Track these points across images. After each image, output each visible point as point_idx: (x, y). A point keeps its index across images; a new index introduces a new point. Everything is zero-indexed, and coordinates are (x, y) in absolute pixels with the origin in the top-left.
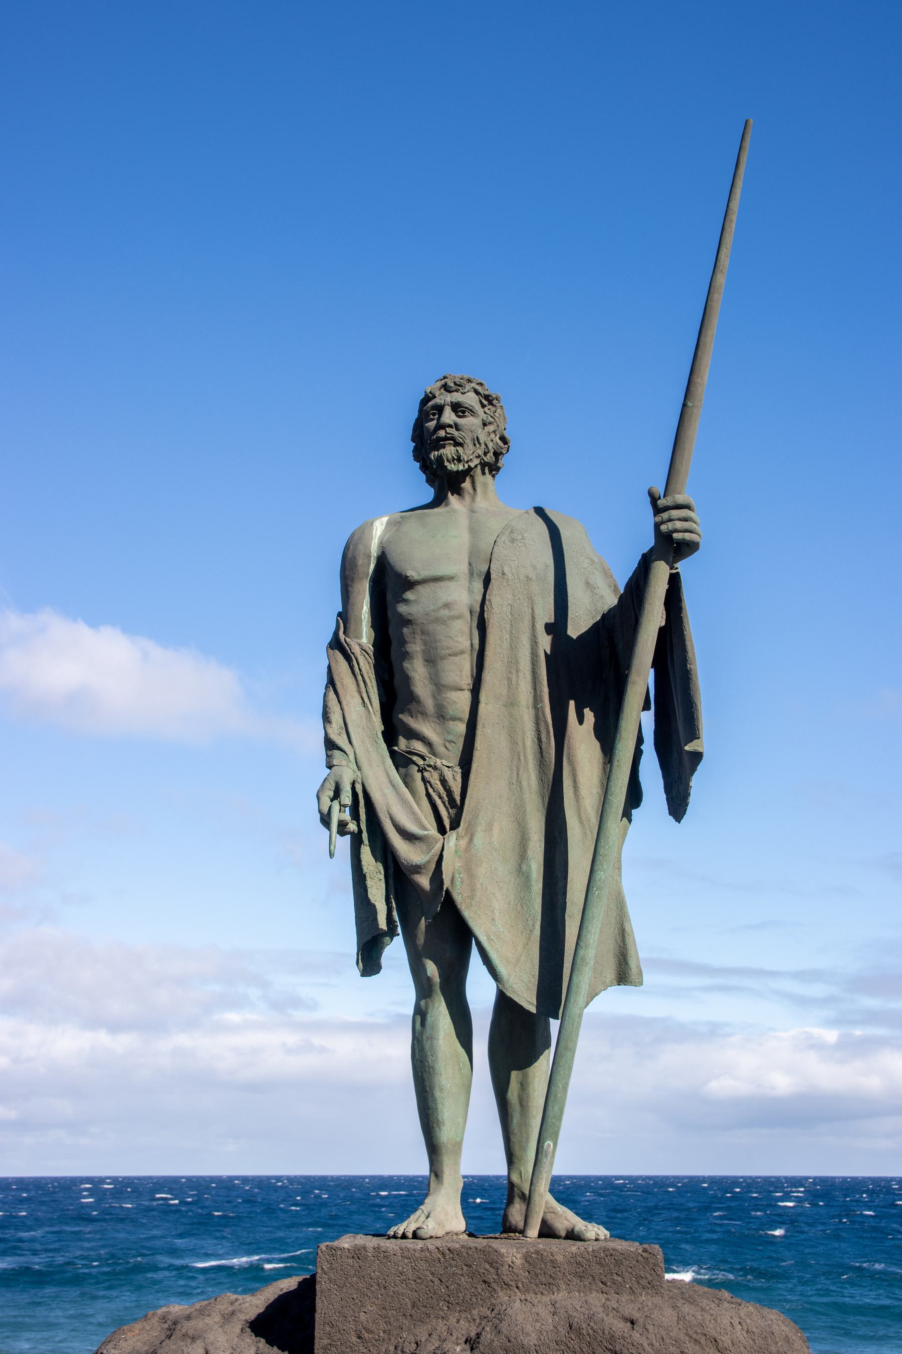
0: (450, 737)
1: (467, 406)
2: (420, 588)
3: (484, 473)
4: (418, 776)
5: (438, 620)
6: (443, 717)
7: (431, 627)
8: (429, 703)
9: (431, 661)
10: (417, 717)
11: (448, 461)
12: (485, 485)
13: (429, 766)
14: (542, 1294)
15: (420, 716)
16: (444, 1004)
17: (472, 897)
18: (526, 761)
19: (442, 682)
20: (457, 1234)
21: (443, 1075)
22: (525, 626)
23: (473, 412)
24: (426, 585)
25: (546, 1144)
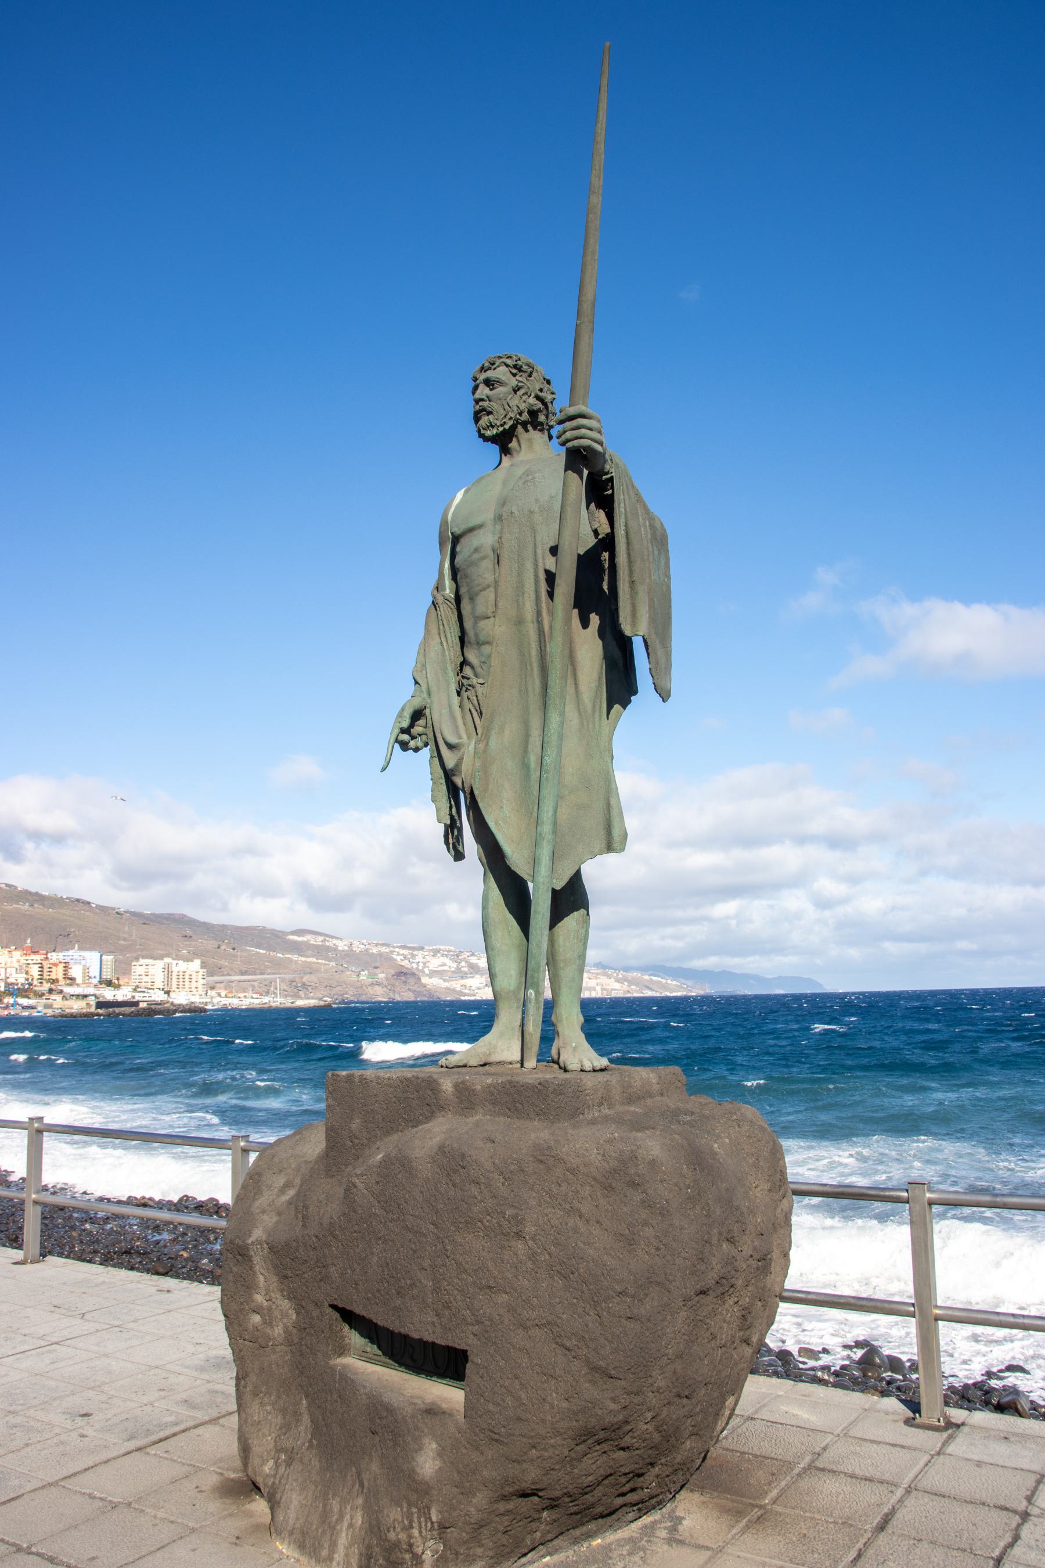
3: (527, 431)
12: (530, 440)
16: (492, 879)
17: (486, 790)
18: (532, 669)
20: (511, 1063)
22: (529, 553)
23: (501, 383)
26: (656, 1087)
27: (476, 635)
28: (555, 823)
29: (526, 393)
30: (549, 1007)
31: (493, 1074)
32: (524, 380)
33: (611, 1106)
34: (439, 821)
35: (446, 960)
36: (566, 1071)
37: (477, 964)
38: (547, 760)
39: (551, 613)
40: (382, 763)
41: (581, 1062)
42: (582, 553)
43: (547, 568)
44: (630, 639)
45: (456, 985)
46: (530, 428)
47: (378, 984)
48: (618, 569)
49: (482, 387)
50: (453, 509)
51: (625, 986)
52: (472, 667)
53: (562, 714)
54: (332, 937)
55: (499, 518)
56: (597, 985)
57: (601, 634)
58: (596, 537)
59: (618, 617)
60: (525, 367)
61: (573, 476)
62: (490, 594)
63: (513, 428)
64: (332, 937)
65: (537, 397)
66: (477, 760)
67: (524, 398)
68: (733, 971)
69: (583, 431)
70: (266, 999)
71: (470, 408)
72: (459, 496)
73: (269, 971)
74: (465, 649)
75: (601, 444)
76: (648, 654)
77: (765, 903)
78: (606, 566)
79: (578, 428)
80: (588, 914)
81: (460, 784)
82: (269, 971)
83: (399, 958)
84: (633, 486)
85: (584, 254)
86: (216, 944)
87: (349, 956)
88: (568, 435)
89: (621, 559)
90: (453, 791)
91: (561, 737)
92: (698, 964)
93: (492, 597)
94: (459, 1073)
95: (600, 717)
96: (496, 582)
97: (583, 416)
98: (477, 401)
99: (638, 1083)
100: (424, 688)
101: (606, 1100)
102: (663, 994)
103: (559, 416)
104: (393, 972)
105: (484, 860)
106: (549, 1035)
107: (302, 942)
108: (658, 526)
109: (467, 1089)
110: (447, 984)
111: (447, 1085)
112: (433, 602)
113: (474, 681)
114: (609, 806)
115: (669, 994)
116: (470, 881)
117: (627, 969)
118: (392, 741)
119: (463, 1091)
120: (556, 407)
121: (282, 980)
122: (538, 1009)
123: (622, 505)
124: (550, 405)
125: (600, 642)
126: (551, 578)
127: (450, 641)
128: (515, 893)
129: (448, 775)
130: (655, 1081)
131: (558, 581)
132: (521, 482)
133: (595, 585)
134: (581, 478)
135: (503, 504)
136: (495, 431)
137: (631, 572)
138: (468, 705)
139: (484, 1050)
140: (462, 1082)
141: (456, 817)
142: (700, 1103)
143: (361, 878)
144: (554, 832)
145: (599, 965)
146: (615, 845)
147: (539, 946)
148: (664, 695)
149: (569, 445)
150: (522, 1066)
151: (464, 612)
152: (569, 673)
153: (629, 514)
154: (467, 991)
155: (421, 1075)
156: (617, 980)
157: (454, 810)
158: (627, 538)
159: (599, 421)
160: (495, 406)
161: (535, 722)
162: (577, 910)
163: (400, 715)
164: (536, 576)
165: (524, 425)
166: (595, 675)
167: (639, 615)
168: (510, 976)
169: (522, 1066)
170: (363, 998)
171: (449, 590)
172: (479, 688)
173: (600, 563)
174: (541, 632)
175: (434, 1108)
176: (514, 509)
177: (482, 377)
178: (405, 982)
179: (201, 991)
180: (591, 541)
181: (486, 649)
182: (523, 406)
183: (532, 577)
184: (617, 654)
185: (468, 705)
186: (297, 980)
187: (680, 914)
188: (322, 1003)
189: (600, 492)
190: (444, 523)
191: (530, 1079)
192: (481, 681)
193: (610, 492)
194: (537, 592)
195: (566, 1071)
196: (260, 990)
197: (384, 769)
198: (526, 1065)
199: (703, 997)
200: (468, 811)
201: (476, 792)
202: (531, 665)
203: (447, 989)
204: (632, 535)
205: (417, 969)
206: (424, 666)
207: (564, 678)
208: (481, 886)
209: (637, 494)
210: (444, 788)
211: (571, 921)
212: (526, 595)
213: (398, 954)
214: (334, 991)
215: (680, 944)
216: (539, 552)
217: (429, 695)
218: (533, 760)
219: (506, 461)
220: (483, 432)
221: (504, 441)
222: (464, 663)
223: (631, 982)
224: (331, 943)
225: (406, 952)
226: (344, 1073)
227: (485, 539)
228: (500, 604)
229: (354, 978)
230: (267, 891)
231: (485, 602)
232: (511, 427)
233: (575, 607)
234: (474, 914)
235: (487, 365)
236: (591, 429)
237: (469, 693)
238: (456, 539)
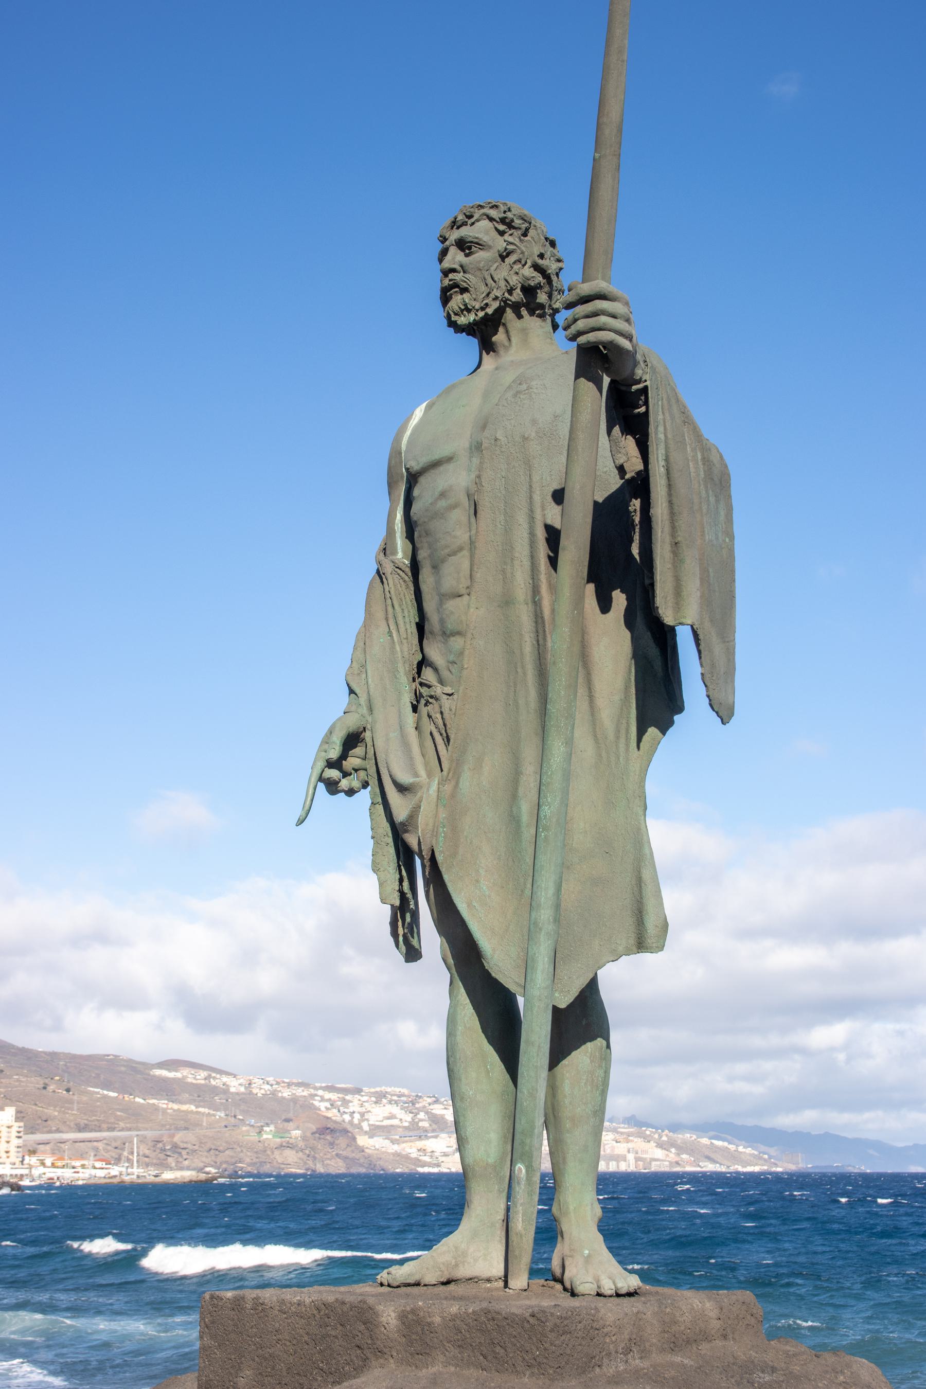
1: (470, 239)
3: (520, 317)
11: (456, 314)
12: (524, 331)
14: (416, 1367)
16: (462, 990)
18: (525, 674)
20: (489, 1280)
21: (463, 1080)
24: (427, 475)
25: (517, 1167)
26: (715, 1325)
27: (442, 621)
28: (557, 906)
29: (519, 261)
30: (549, 1191)
31: (461, 1298)
32: (517, 242)
33: (644, 1354)
34: (383, 901)
35: (395, 1110)
36: (573, 1294)
37: (442, 1117)
38: (546, 810)
39: (553, 589)
40: (298, 813)
41: (598, 1281)
42: (600, 500)
43: (549, 522)
44: (672, 629)
45: (411, 1149)
46: (524, 312)
47: (290, 1146)
48: (654, 525)
49: (453, 250)
50: (408, 433)
51: (672, 1155)
52: (436, 670)
53: (569, 742)
54: (221, 1072)
55: (477, 447)
56: (627, 1152)
57: (629, 620)
58: (622, 478)
59: (654, 597)
60: (517, 222)
61: (587, 386)
62: (463, 561)
63: (500, 312)
64: (221, 1072)
65: (536, 267)
66: (441, 809)
67: (517, 267)
68: (843, 1134)
69: (603, 319)
70: (115, 1171)
71: (436, 283)
72: (419, 413)
73: (122, 1124)
74: (425, 642)
75: (630, 338)
76: (699, 652)
77: (891, 1026)
78: (637, 519)
79: (595, 314)
80: (608, 1046)
81: (415, 847)
82: (122, 1124)
83: (323, 1106)
84: (678, 400)
85: (607, 54)
86: (41, 1082)
87: (247, 1102)
88: (581, 325)
89: (659, 510)
90: (405, 855)
91: (567, 776)
92: (787, 1121)
93: (466, 564)
94: (408, 1295)
95: (627, 745)
96: (472, 542)
97: (602, 297)
98: (446, 273)
99: (687, 1318)
100: (363, 700)
101: (636, 1344)
102: (732, 1169)
103: (568, 297)
104: (314, 1128)
105: (451, 961)
106: (548, 1233)
107: (174, 1080)
108: (715, 458)
109: (419, 1322)
110: (396, 1148)
111: (389, 1316)
112: (378, 572)
113: (438, 690)
114: (639, 881)
115: (740, 1169)
116: (429, 989)
117: (675, 1128)
118: (314, 778)
119: (413, 1323)
120: (564, 281)
121: (142, 1140)
122: (530, 1194)
123: (661, 429)
124: (554, 278)
125: (628, 634)
126: (553, 537)
127: (402, 629)
128: (499, 1016)
129: (398, 832)
130: (713, 1314)
131: (563, 542)
132: (509, 395)
133: (617, 550)
134: (600, 390)
135: (484, 427)
136: (472, 317)
137: (673, 528)
138: (428, 727)
139: (448, 1258)
140: (413, 1311)
141: (409, 895)
142: (786, 1353)
143: (267, 981)
144: (557, 920)
145: (631, 1120)
146: (650, 941)
147: (533, 1095)
148: (723, 712)
149: (582, 339)
150: (506, 1285)
151: (424, 587)
152: (580, 680)
153: (671, 442)
154: (427, 1159)
155: (349, 1299)
156: (660, 1145)
157: (406, 884)
158: (669, 478)
159: (627, 304)
160: (472, 280)
161: (529, 754)
162: (592, 1039)
163: (326, 740)
164: (532, 534)
165: (516, 307)
166: (619, 683)
167: (684, 593)
168: (488, 1144)
169: (506, 1285)
170: (267, 1169)
171: (401, 553)
172: (446, 702)
173: (628, 515)
174: (538, 618)
175: (368, 1353)
176: (499, 435)
177: (454, 235)
178: (332, 1144)
179: (14, 1157)
180: (615, 483)
181: (457, 643)
182: (514, 280)
183: (526, 535)
184: (653, 651)
185: (428, 727)
186: (165, 1139)
187: (757, 1042)
188: (202, 1176)
189: (628, 410)
190: (396, 453)
191: (518, 1307)
192: (448, 690)
193: (643, 409)
194: (533, 557)
195: (573, 1294)
196: (107, 1155)
197: (301, 822)
198: (512, 1283)
199: (791, 1175)
200: (427, 885)
201: (440, 858)
202: (523, 667)
203: (397, 1154)
204: (675, 474)
205: (351, 1122)
206: (364, 666)
207: (572, 687)
208: (445, 1002)
209: (684, 412)
210: (392, 850)
211: (581, 1058)
212: (516, 562)
213: (323, 1099)
214: (222, 1157)
215: (758, 1089)
216: (537, 498)
217: (371, 709)
218: (525, 809)
219: (489, 361)
220: (454, 318)
221: (484, 332)
222: (423, 663)
223: (681, 1149)
224: (218, 1081)
225: (333, 1096)
226: (229, 1294)
227: (456, 478)
228: (478, 576)
229: (253, 1137)
230: (123, 999)
231: (454, 572)
232: (496, 311)
233: (588, 582)
234: (437, 1037)
235: (461, 217)
236: (614, 316)
237: (430, 707)
238: (413, 478)
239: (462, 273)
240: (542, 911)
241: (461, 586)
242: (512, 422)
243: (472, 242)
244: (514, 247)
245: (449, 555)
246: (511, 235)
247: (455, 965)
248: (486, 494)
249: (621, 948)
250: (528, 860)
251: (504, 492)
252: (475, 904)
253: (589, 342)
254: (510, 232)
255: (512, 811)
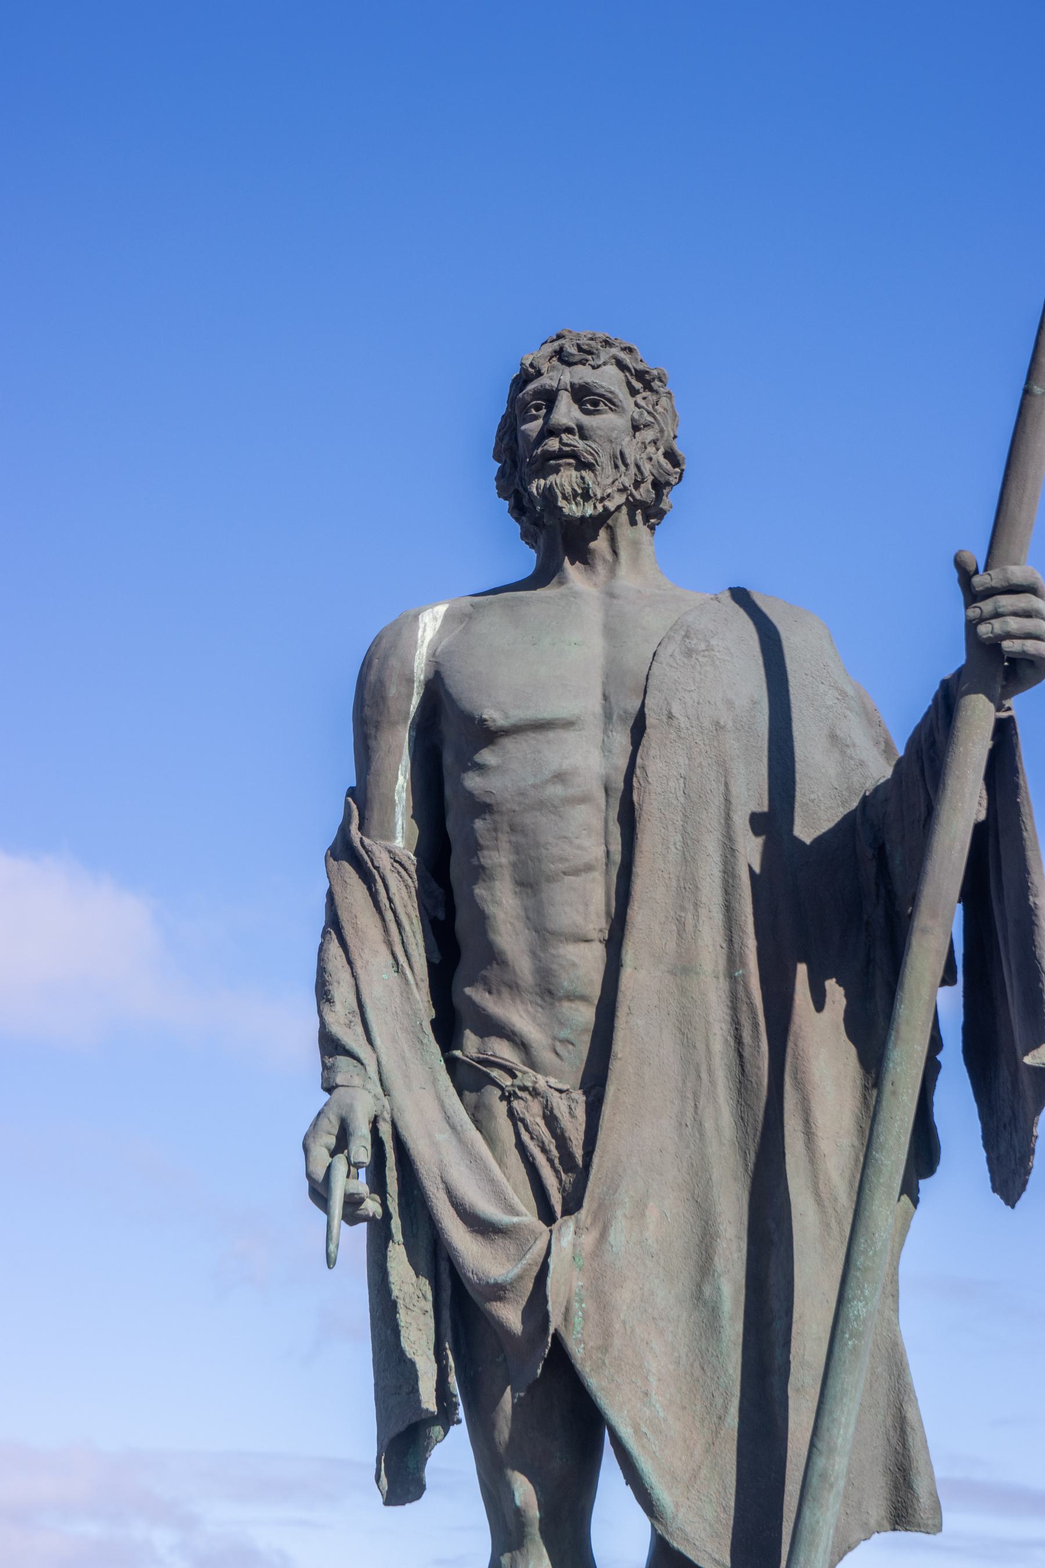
0: (564, 1033)
2: (508, 743)
3: (633, 523)
4: (501, 1108)
5: (541, 805)
6: (550, 993)
7: (529, 819)
8: (523, 965)
9: (530, 883)
10: (499, 993)
11: (565, 498)
12: (635, 544)
13: (524, 1088)
15: (505, 990)
18: (712, 1083)
19: (551, 926)
23: (613, 404)
146: (923, 1513)
212: (702, 911)
239: (577, 437)
240: (837, 1459)
241: (591, 926)
242: (694, 695)
243: (602, 396)
244: (651, 419)
245: (565, 873)
246: (644, 398)
247: (541, 1520)
248: (653, 796)
249: (872, 1522)
250: (731, 1371)
251: (682, 799)
252: (645, 1430)
253: (1024, 652)
254: (644, 394)
255: (701, 1291)
